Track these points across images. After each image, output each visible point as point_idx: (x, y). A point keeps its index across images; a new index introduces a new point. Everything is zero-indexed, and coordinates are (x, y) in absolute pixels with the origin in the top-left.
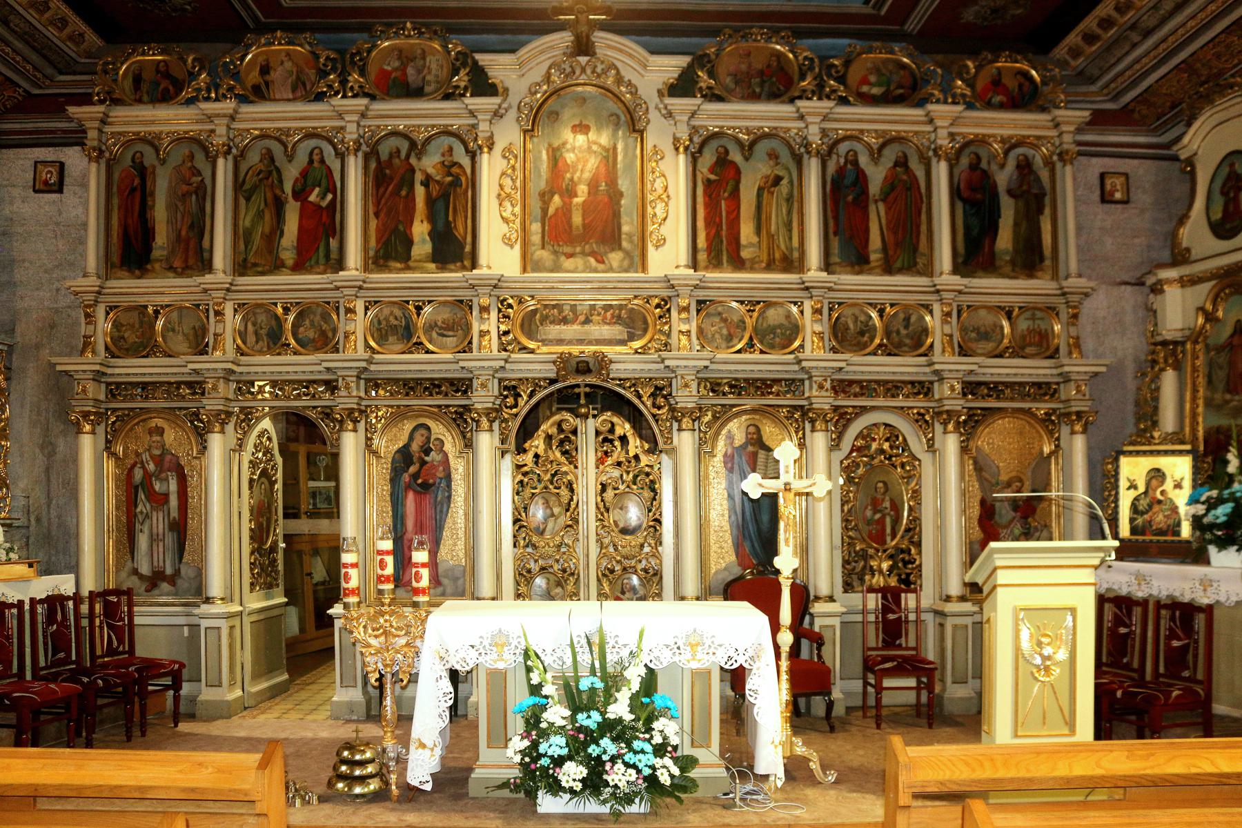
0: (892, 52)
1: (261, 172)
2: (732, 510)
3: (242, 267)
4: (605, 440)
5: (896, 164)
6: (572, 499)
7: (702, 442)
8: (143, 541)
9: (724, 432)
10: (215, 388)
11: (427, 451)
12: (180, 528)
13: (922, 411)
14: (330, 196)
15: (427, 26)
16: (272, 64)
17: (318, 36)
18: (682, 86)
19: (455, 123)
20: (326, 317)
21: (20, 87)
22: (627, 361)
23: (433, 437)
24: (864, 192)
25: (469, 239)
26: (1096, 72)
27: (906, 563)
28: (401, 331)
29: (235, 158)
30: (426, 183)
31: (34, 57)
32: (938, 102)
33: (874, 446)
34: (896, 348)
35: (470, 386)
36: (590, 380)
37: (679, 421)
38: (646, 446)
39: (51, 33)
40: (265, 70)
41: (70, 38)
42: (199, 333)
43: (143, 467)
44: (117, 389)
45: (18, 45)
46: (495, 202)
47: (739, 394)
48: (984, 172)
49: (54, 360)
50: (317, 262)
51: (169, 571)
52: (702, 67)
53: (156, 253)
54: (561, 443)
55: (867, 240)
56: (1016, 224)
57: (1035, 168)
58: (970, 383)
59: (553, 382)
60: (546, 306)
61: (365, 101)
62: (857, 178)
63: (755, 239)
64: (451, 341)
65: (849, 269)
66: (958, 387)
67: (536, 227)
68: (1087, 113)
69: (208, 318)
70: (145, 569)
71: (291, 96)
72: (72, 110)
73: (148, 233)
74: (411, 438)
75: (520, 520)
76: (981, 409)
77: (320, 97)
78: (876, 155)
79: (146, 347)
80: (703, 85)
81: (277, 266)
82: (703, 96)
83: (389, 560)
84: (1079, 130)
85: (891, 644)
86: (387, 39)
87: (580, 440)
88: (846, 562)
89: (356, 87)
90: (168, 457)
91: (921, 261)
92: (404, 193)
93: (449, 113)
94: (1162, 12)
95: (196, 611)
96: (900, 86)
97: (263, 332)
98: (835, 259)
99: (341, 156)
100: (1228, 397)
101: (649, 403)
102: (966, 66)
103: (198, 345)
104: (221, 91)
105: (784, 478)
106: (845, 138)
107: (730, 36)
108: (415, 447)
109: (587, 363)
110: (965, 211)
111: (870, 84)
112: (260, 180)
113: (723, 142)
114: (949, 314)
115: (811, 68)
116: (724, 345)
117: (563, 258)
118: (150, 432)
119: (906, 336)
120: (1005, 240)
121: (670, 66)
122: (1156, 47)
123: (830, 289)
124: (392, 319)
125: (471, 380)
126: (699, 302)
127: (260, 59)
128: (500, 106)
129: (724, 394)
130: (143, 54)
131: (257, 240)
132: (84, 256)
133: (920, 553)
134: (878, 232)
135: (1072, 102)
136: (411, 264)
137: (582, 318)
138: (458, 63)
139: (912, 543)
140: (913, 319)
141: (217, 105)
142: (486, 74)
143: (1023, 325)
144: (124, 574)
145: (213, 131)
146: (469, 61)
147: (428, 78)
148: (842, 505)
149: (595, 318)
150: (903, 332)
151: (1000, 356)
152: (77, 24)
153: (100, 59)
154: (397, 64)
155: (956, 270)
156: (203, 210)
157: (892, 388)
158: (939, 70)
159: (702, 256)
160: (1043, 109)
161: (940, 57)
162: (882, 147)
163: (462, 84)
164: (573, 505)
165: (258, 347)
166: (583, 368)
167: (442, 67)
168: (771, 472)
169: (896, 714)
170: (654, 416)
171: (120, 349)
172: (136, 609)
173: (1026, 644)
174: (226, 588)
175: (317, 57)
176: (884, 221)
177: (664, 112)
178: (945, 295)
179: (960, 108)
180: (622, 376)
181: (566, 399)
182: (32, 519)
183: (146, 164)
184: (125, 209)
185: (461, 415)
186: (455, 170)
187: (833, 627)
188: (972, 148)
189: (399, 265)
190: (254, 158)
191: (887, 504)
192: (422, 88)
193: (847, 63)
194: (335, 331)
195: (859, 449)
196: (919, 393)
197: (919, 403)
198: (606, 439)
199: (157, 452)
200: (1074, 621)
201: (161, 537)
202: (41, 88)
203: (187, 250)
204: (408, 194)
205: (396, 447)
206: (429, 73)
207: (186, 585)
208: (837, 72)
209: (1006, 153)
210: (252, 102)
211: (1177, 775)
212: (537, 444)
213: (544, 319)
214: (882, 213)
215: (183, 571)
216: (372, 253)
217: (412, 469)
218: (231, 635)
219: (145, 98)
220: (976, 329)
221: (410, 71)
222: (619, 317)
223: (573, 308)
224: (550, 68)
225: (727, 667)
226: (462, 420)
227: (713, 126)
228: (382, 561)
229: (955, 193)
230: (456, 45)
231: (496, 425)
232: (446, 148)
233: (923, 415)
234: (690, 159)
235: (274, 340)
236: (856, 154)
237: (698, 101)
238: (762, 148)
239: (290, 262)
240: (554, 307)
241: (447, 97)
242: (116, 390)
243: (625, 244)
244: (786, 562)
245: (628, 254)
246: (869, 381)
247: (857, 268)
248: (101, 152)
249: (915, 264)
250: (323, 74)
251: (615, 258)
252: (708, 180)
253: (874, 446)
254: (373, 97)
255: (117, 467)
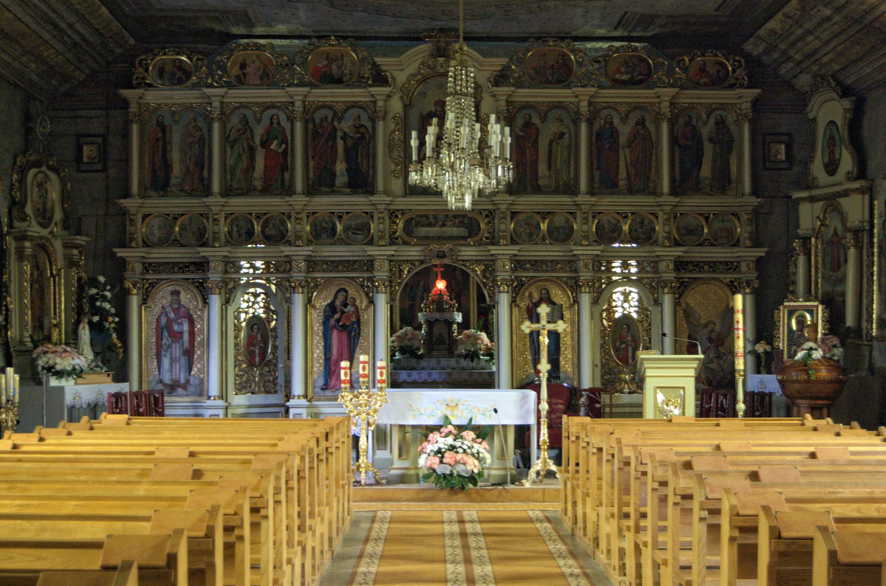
5: (637, 124)
8: (166, 362)
14: (284, 146)
23: (349, 296)
24: (616, 142)
30: (344, 138)
36: (446, 261)
40: (243, 66)
51: (182, 381)
56: (714, 161)
59: (422, 262)
63: (547, 173)
71: (259, 82)
73: (167, 167)
74: (336, 297)
92: (330, 144)
97: (243, 231)
99: (291, 120)
100: (831, 273)
102: (684, 60)
106: (605, 108)
108: (338, 303)
111: (621, 73)
112: (240, 135)
120: (706, 171)
124: (324, 223)
130: (165, 54)
131: (239, 174)
137: (440, 223)
143: (717, 225)
149: (449, 223)
151: (701, 245)
154: (325, 63)
156: (203, 153)
158: (666, 63)
168: (534, 319)
170: (484, 283)
176: (628, 160)
186: (362, 130)
191: (629, 338)
199: (176, 306)
207: (193, 389)
214: (628, 155)
217: (336, 316)
220: (686, 228)
221: (334, 67)
222: (463, 222)
223: (435, 217)
229: (674, 141)
236: (612, 118)
239: (259, 187)
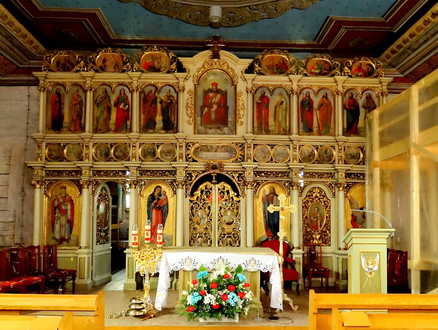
0: (323, 57)
1: (102, 97)
2: (265, 217)
3: (96, 130)
4: (222, 192)
5: (323, 97)
6: (210, 213)
7: (255, 192)
8: (57, 227)
9: (262, 189)
10: (85, 172)
11: (160, 195)
12: (71, 222)
13: (331, 183)
14: (127, 106)
15: (162, 47)
16: (107, 59)
17: (124, 49)
18: (250, 70)
19: (172, 82)
20: (125, 149)
21: (15, 64)
22: (230, 166)
25: (176, 122)
26: (395, 64)
27: (325, 236)
28: (152, 153)
29: (94, 92)
30: (161, 102)
31: (21, 54)
32: (339, 75)
33: (314, 195)
34: (322, 161)
35: (175, 173)
36: (217, 171)
37: (247, 186)
38: (236, 194)
39: (27, 46)
40: (104, 61)
41: (34, 47)
42: (80, 153)
43: (58, 200)
44: (49, 172)
45: (16, 50)
46: (185, 110)
47: (268, 177)
48: (355, 100)
49: (26, 162)
50: (123, 129)
51: (66, 238)
52: (257, 63)
53: (64, 125)
54: (207, 192)
55: (312, 124)
57: (372, 98)
58: (348, 173)
59: (204, 172)
60: (202, 146)
61: (140, 73)
62: (309, 102)
64: (169, 157)
65: (306, 133)
66: (344, 175)
67: (199, 119)
68: (392, 79)
69: (83, 148)
70: (58, 237)
72: (34, 73)
73: (62, 117)
75: (192, 219)
76: (352, 182)
77: (124, 71)
78: (316, 94)
79: (61, 158)
80: (257, 69)
81: (108, 130)
82: (257, 73)
83: (149, 232)
84: (389, 84)
85: (312, 260)
86: (148, 51)
87: (213, 192)
88: (304, 235)
89: (137, 68)
90: (67, 197)
91: (331, 131)
93: (170, 79)
94: (419, 43)
95: (76, 252)
96: (325, 70)
97: (103, 153)
98: (301, 130)
99: (131, 92)
101: (237, 180)
103: (79, 158)
104: (88, 68)
105: (281, 206)
106: (306, 88)
107: (267, 52)
109: (216, 165)
110: (347, 113)
111: (315, 69)
112: (102, 100)
113: (264, 89)
114: (341, 149)
115: (294, 63)
116: (262, 160)
117: (208, 129)
118: (61, 188)
119: (326, 157)
121: (246, 63)
122: (417, 55)
123: (299, 141)
125: (176, 171)
126: (254, 145)
127: (103, 57)
128: (187, 76)
129: (262, 177)
131: (101, 121)
132: (38, 125)
133: (330, 233)
134: (317, 123)
135: (386, 74)
136: (156, 130)
137: (214, 150)
138: (172, 61)
139: (327, 229)
140: (328, 151)
141: (87, 73)
142: (182, 64)
144: (50, 239)
145: (85, 82)
146: (176, 60)
147: (162, 65)
148: (303, 215)
150: (325, 155)
151: (359, 164)
152: (36, 42)
153: (45, 55)
154: (151, 60)
155: (344, 134)
156: (81, 109)
157: (321, 175)
159: (256, 129)
160: (376, 77)
161: (340, 59)
162: (319, 91)
163: (174, 68)
164: (210, 215)
165: (101, 158)
166: (214, 167)
167: (167, 61)
169: (81, 119)
171: (51, 158)
172: (58, 251)
173: (363, 265)
174: (87, 243)
175: (123, 57)
176: (318, 117)
177: (243, 79)
178: (340, 143)
179: (347, 77)
180: (228, 170)
181: (208, 178)
182: (16, 219)
183: (61, 93)
184: (53, 109)
185: (172, 183)
187: (300, 258)
188: (350, 91)
189: (151, 131)
190: (100, 92)
191: (319, 215)
192: (160, 69)
193: (307, 62)
194: (128, 153)
195: (309, 196)
196: (330, 177)
197: (330, 180)
198: (222, 192)
199: (63, 195)
200: (380, 256)
201: (64, 225)
202: (22, 65)
203: (75, 124)
204: (154, 107)
205: (149, 194)
206: (162, 63)
208: (303, 65)
209: (362, 93)
210: (100, 72)
211: (405, 305)
212: (198, 193)
213: (201, 150)
214: (318, 115)
215: (71, 238)
216: (142, 127)
217: (155, 202)
218: (88, 260)
219: (61, 70)
220: (351, 155)
221: (156, 63)
224: (204, 63)
225: (263, 271)
226: (173, 184)
227: (260, 83)
228: (147, 233)
229: (344, 107)
230: (172, 54)
231: (184, 187)
232: (168, 90)
233: (331, 184)
234: (252, 96)
235: (107, 157)
237: (255, 75)
238: (277, 91)
239: (113, 129)
240: (205, 146)
241: (168, 72)
242: (50, 173)
243: (229, 125)
244: (282, 234)
245: (230, 129)
246: (312, 173)
247: (309, 133)
248: (45, 89)
249: (329, 132)
250: (125, 63)
251: (226, 129)
252: (258, 103)
253: (314, 195)
254: (143, 72)
255: (48, 200)
